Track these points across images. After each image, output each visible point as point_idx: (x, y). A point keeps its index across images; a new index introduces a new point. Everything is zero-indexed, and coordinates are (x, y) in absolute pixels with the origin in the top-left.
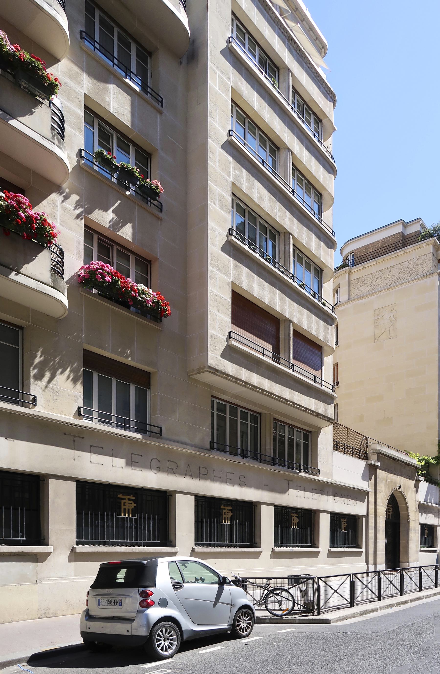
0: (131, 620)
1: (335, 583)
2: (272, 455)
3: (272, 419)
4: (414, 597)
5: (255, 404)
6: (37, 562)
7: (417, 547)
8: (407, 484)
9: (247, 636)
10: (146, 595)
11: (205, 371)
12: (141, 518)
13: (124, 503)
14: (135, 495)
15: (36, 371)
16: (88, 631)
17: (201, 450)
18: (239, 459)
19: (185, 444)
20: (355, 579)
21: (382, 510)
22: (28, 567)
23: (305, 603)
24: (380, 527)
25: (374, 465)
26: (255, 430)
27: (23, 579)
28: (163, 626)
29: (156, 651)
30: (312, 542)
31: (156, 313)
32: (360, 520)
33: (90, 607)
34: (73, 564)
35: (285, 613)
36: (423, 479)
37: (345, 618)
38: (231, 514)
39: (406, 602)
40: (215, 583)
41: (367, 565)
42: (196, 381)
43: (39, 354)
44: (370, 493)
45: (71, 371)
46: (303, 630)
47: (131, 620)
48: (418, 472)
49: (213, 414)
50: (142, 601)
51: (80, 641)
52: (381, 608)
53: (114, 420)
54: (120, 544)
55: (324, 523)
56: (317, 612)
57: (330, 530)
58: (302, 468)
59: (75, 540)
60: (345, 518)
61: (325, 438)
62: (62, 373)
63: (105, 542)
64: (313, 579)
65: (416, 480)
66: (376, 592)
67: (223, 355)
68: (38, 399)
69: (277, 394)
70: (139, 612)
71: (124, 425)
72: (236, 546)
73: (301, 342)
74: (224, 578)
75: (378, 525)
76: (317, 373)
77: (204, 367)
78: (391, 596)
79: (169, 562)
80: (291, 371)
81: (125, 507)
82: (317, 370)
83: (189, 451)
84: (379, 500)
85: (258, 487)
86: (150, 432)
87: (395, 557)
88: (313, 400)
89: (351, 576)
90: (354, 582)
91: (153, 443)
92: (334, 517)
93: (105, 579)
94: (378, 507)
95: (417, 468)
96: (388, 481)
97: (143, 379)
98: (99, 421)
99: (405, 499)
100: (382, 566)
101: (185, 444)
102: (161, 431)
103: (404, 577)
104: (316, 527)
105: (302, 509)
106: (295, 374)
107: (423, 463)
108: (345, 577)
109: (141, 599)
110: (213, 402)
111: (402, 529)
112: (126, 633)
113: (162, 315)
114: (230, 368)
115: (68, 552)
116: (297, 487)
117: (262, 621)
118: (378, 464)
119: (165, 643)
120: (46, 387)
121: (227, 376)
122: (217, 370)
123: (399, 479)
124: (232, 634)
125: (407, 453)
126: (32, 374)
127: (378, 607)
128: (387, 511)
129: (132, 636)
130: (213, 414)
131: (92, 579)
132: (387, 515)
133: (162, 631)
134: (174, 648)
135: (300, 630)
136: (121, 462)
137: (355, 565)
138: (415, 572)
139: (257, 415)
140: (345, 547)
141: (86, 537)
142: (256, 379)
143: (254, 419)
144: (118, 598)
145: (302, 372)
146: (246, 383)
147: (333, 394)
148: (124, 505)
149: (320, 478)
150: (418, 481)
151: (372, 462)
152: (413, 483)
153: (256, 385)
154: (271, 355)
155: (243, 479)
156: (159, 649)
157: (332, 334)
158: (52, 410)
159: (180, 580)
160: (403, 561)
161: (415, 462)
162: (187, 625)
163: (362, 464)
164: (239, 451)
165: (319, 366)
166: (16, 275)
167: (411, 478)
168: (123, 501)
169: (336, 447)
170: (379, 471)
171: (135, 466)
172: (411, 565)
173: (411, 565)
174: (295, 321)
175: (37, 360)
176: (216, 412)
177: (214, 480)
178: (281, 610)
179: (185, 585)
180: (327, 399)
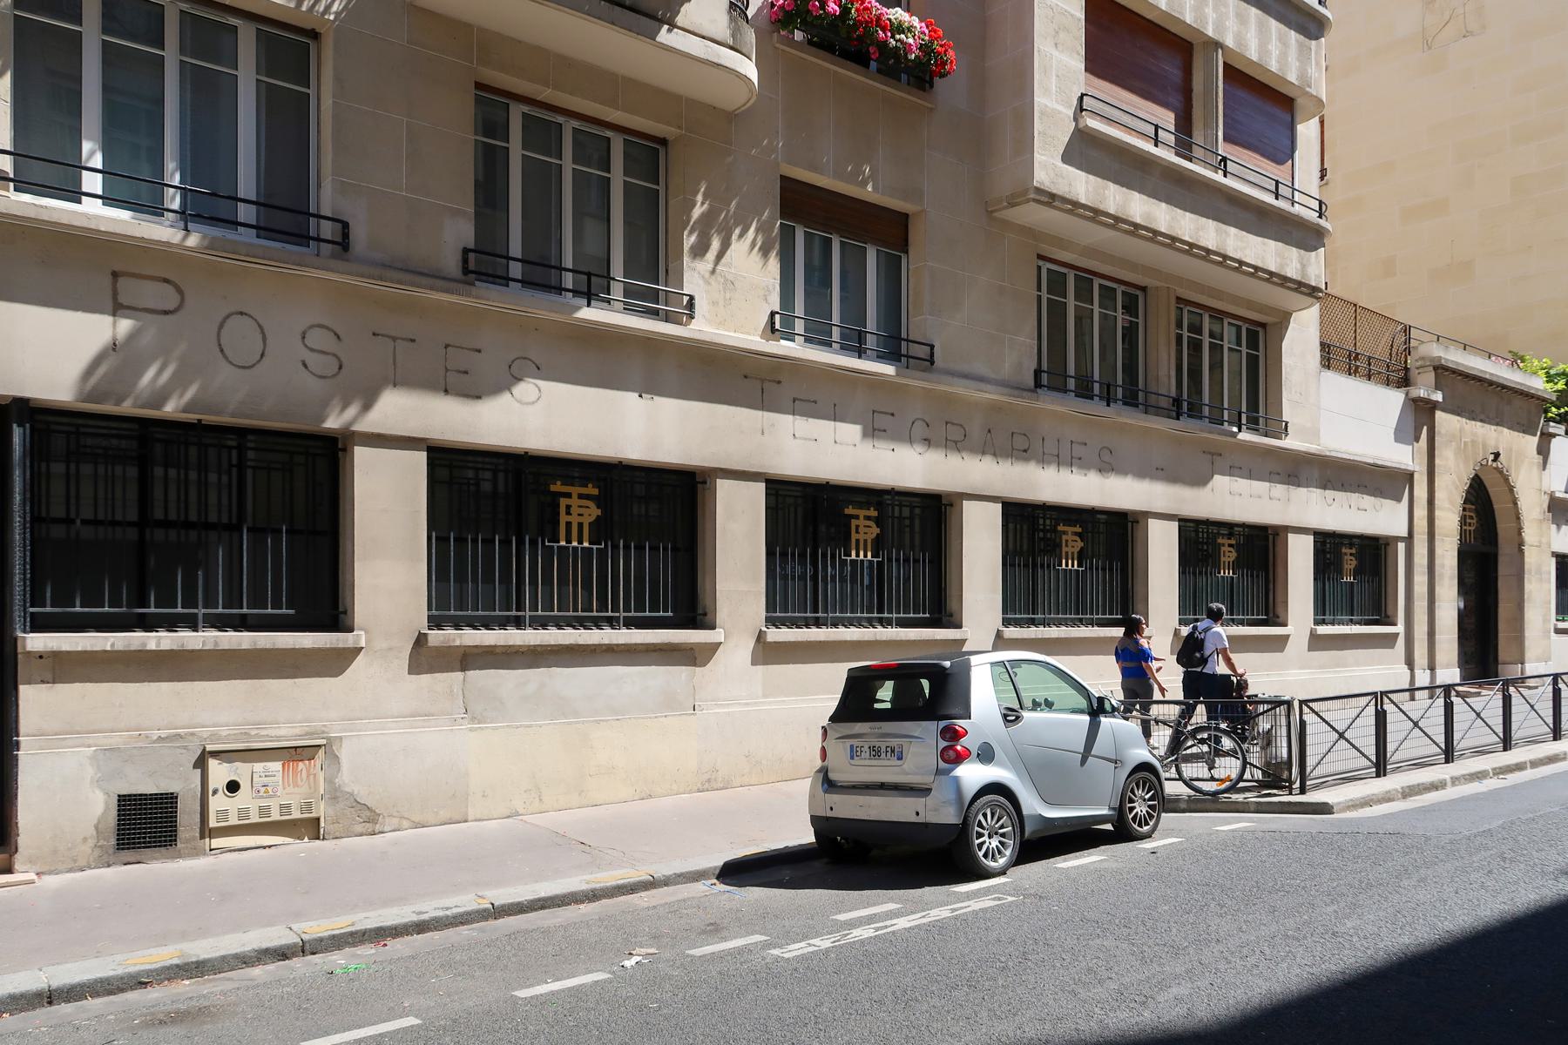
0: (924, 791)
1: (1339, 714)
2: (1173, 393)
3: (1173, 301)
4: (1541, 755)
5: (1134, 266)
6: (695, 665)
7: (1546, 620)
8: (1517, 446)
9: (1148, 836)
10: (953, 735)
11: (1028, 201)
12: (890, 560)
13: (568, 507)
14: (879, 506)
15: (693, 238)
16: (830, 814)
17: (1016, 392)
18: (1096, 407)
19: (981, 379)
20: (1388, 707)
21: (1449, 519)
22: (680, 673)
23: (1268, 764)
24: (1443, 566)
25: (1427, 401)
26: (1130, 333)
27: (669, 704)
28: (986, 805)
29: (974, 857)
30: (324, 603)
31: (920, 73)
32: (1390, 550)
33: (829, 762)
34: (760, 668)
35: (1224, 786)
36: (1561, 429)
37: (1367, 802)
38: (1080, 544)
39: (1519, 767)
40: (1081, 712)
41: (1412, 669)
42: (1006, 224)
43: (700, 198)
44: (1416, 476)
45: (757, 231)
46: (1273, 827)
47: (924, 791)
48: (1546, 411)
49: (1179, 338)
50: (944, 749)
51: (807, 837)
52: (1455, 781)
53: (836, 333)
54: (849, 623)
55: (1300, 558)
56: (1297, 785)
57: (770, 554)
58: (1244, 421)
59: (762, 613)
60: (1351, 546)
61: (1302, 337)
62: (741, 236)
63: (244, 616)
64: (1289, 704)
65: (1542, 434)
66: (1371, 751)
67: (1067, 158)
68: (697, 302)
69: (1187, 238)
70: (938, 772)
71: (855, 343)
72: (1091, 623)
73: (1242, 94)
74: (1101, 700)
75: (1438, 562)
76: (1279, 172)
77: (1026, 191)
78: (1480, 751)
79: (993, 664)
80: (1218, 177)
81: (569, 518)
82: (1280, 162)
83: (991, 395)
84: (1440, 495)
85: (1142, 472)
86: (908, 356)
87: (1484, 647)
88: (1272, 243)
89: (1379, 697)
90: (1385, 712)
91: (916, 382)
92: (1324, 543)
93: (855, 703)
94: (1437, 513)
95: (1544, 400)
96: (1464, 440)
97: (890, 230)
98: (808, 340)
99: (1511, 489)
100: (1450, 673)
101: (981, 379)
102: (932, 355)
103: (1389, 718)
104: (1280, 570)
105: (1243, 525)
106: (1229, 182)
107: (1561, 385)
108: (1363, 701)
109: (943, 744)
110: (1039, 268)
111: (1503, 570)
112: (914, 819)
113: (933, 74)
114: (1081, 185)
115: (751, 644)
116: (1232, 471)
117: (1172, 805)
118: (1438, 397)
119: (992, 845)
120: (713, 272)
121: (1074, 206)
122: (1053, 196)
123: (1494, 435)
124: (1122, 832)
125: (1516, 359)
126: (686, 247)
127: (1447, 777)
128: (1463, 521)
129: (926, 825)
130: (1179, 338)
131: (831, 702)
132: (1462, 533)
133: (985, 815)
134: (1008, 853)
135: (1265, 827)
136: (852, 431)
137: (1380, 670)
138: (1541, 689)
139: (1138, 292)
140: (1352, 622)
141: (461, 606)
142: (1139, 207)
143: (1131, 307)
144: (894, 742)
145: (1247, 175)
146: (1117, 219)
147: (1322, 222)
148: (568, 513)
149: (1290, 442)
150: (1547, 437)
151: (1422, 393)
152: (1533, 441)
153: (1138, 220)
154: (1171, 139)
155: (1106, 457)
156: (981, 854)
157: (1318, 63)
158: (721, 324)
159: (1016, 706)
160: (1508, 660)
161: (1538, 384)
162: (1032, 805)
163: (1394, 399)
164: (1071, 383)
165: (1283, 152)
166: (669, 31)
167: (1528, 429)
168: (563, 502)
169: (1329, 356)
170: (1439, 414)
171: (879, 438)
172: (1531, 668)
173: (1531, 668)
174: (1229, 42)
175: (697, 212)
176: (1186, 334)
177: (1043, 460)
178: (1213, 779)
179: (1026, 714)
180: (1306, 235)
